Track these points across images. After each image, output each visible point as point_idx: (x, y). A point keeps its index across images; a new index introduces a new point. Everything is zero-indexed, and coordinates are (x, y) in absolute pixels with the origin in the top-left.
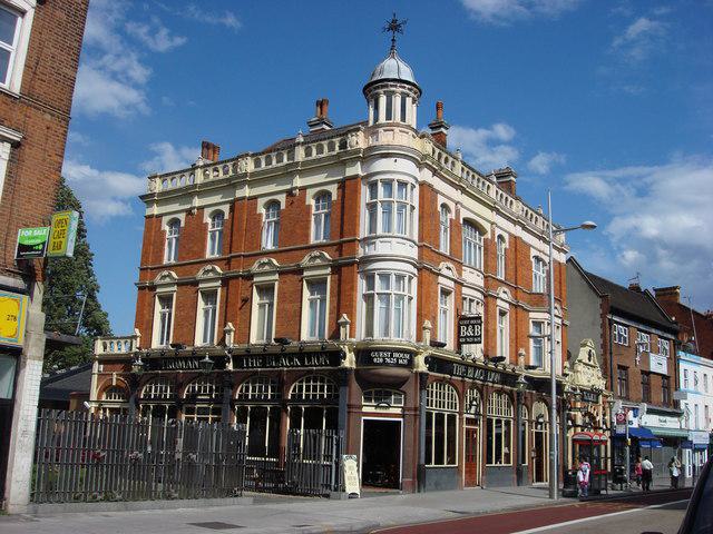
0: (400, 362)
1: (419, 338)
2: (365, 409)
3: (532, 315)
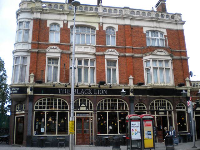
0: (14, 92)
1: (29, 81)
2: (17, 113)
3: (145, 58)
